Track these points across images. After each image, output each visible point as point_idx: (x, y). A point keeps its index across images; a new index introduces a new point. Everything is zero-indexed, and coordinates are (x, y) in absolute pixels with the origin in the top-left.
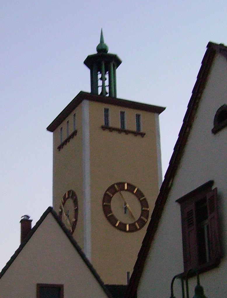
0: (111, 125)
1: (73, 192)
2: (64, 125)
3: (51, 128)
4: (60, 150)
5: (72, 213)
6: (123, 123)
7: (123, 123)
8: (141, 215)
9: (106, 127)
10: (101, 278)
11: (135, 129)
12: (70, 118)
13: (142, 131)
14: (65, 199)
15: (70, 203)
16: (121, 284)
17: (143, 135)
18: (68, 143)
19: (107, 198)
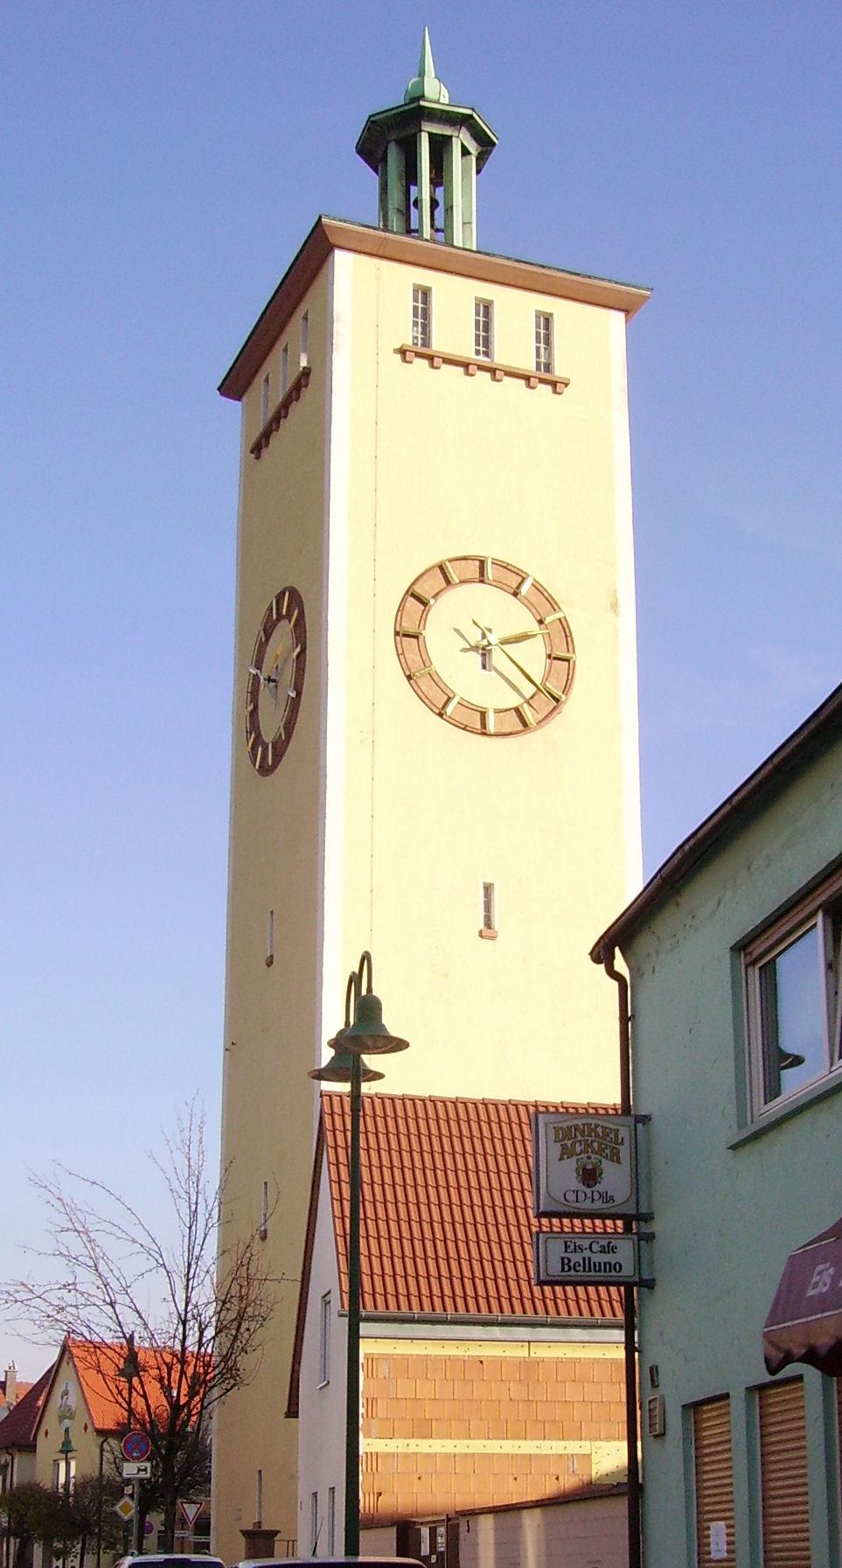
3: (235, 384)
4: (258, 458)
6: (484, 340)
7: (484, 340)
9: (421, 351)
11: (528, 364)
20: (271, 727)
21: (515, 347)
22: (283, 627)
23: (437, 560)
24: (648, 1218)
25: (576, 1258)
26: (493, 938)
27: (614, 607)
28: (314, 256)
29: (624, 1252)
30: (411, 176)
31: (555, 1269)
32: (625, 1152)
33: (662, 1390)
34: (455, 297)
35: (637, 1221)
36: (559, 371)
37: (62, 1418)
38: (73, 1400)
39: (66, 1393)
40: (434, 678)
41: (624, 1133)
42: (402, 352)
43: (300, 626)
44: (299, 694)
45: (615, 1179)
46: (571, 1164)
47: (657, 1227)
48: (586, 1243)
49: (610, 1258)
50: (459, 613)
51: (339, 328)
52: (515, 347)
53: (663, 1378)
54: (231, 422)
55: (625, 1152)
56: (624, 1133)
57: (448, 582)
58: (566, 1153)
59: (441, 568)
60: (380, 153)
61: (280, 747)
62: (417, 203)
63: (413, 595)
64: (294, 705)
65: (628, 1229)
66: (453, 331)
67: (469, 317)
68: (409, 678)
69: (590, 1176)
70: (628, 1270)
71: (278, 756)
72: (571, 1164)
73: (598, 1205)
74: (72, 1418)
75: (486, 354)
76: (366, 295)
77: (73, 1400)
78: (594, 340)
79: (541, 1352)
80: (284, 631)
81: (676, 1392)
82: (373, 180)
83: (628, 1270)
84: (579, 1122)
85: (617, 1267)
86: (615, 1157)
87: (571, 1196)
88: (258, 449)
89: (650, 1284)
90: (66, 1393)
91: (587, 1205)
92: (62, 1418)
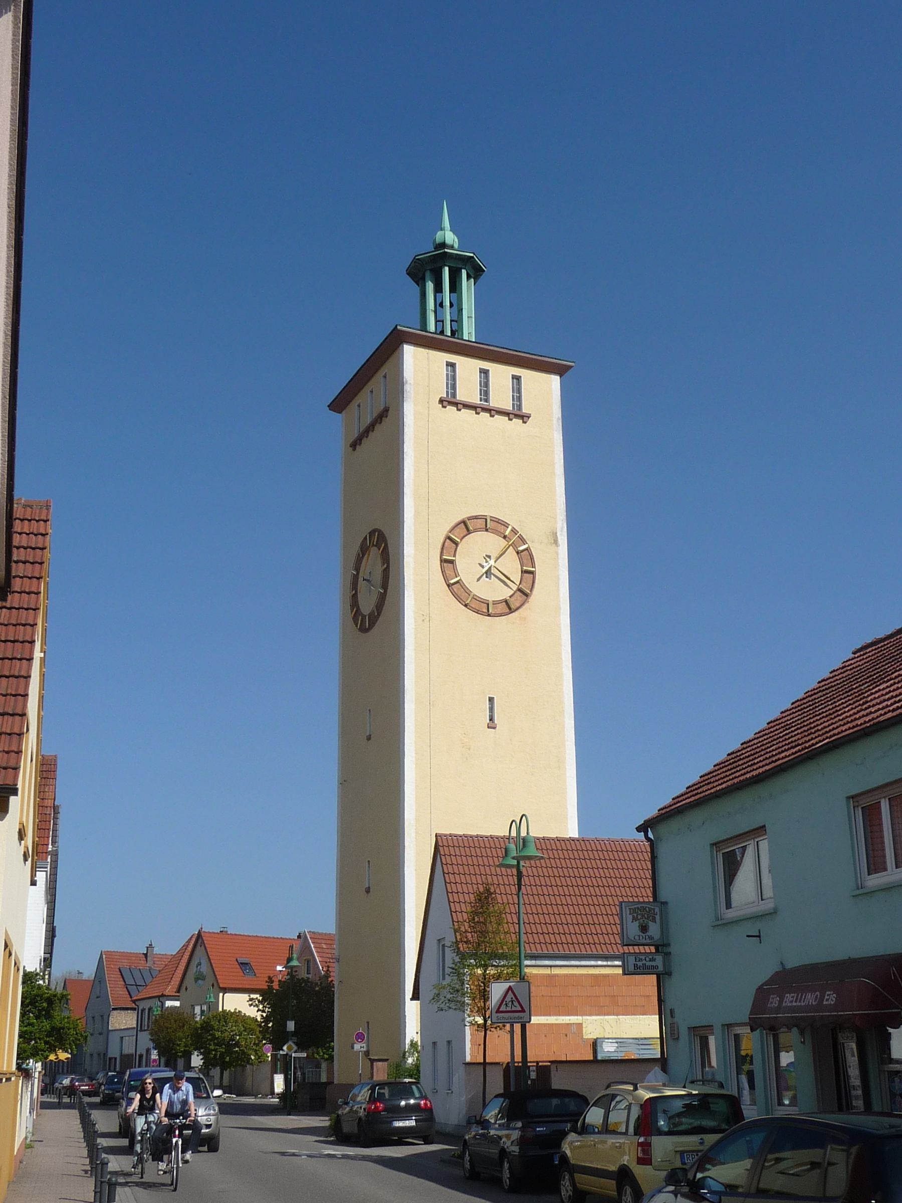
0: (461, 396)
1: (380, 531)
2: (364, 397)
3: (339, 404)
4: (354, 449)
5: (378, 577)
6: (485, 393)
7: (485, 393)
8: (522, 566)
9: (450, 401)
10: (22, 282)
11: (508, 406)
12: (377, 383)
13: (525, 410)
14: (364, 549)
15: (374, 554)
16: (33, 36)
17: (524, 418)
18: (370, 433)
19: (451, 542)
20: (367, 605)
21: (501, 397)
22: (375, 553)
23: (460, 519)
24: (668, 945)
25: (640, 964)
26: (494, 728)
27: (556, 542)
28: (393, 343)
29: (659, 961)
30: (438, 289)
31: (631, 968)
32: (658, 917)
33: (675, 1020)
34: (468, 369)
35: (662, 947)
36: (525, 410)
37: (196, 979)
38: (204, 968)
39: (199, 964)
40: (475, 598)
41: (657, 910)
42: (441, 401)
43: (385, 557)
44: (386, 591)
45: (654, 930)
46: (637, 924)
47: (673, 949)
48: (643, 958)
49: (653, 963)
50: (474, 552)
51: (407, 388)
52: (501, 397)
53: (677, 1013)
54: (338, 428)
55: (658, 917)
56: (657, 910)
57: (468, 529)
58: (635, 919)
59: (464, 522)
60: (421, 275)
61: (374, 618)
62: (441, 305)
63: (510, 608)
64: (382, 598)
65: (657, 950)
66: (469, 391)
67: (477, 377)
68: (466, 606)
69: (644, 929)
70: (661, 968)
71: (372, 624)
72: (637, 924)
73: (648, 941)
74: (204, 979)
75: (486, 401)
76: (419, 366)
77: (204, 968)
78: (544, 391)
79: (556, 971)
80: (374, 553)
81: (684, 1022)
82: (417, 289)
83: (661, 968)
84: (639, 906)
85: (657, 967)
86: (654, 920)
87: (637, 938)
88: (354, 445)
89: (669, 974)
90: (199, 964)
91: (644, 941)
92: (196, 979)
